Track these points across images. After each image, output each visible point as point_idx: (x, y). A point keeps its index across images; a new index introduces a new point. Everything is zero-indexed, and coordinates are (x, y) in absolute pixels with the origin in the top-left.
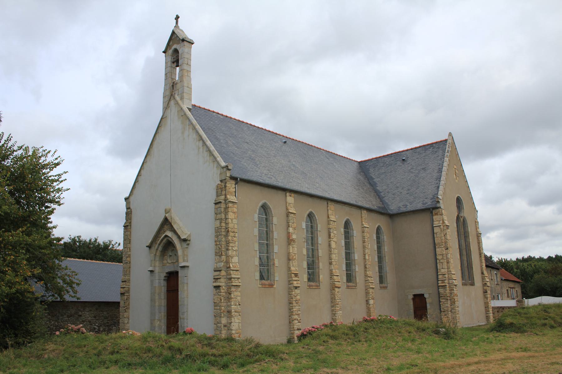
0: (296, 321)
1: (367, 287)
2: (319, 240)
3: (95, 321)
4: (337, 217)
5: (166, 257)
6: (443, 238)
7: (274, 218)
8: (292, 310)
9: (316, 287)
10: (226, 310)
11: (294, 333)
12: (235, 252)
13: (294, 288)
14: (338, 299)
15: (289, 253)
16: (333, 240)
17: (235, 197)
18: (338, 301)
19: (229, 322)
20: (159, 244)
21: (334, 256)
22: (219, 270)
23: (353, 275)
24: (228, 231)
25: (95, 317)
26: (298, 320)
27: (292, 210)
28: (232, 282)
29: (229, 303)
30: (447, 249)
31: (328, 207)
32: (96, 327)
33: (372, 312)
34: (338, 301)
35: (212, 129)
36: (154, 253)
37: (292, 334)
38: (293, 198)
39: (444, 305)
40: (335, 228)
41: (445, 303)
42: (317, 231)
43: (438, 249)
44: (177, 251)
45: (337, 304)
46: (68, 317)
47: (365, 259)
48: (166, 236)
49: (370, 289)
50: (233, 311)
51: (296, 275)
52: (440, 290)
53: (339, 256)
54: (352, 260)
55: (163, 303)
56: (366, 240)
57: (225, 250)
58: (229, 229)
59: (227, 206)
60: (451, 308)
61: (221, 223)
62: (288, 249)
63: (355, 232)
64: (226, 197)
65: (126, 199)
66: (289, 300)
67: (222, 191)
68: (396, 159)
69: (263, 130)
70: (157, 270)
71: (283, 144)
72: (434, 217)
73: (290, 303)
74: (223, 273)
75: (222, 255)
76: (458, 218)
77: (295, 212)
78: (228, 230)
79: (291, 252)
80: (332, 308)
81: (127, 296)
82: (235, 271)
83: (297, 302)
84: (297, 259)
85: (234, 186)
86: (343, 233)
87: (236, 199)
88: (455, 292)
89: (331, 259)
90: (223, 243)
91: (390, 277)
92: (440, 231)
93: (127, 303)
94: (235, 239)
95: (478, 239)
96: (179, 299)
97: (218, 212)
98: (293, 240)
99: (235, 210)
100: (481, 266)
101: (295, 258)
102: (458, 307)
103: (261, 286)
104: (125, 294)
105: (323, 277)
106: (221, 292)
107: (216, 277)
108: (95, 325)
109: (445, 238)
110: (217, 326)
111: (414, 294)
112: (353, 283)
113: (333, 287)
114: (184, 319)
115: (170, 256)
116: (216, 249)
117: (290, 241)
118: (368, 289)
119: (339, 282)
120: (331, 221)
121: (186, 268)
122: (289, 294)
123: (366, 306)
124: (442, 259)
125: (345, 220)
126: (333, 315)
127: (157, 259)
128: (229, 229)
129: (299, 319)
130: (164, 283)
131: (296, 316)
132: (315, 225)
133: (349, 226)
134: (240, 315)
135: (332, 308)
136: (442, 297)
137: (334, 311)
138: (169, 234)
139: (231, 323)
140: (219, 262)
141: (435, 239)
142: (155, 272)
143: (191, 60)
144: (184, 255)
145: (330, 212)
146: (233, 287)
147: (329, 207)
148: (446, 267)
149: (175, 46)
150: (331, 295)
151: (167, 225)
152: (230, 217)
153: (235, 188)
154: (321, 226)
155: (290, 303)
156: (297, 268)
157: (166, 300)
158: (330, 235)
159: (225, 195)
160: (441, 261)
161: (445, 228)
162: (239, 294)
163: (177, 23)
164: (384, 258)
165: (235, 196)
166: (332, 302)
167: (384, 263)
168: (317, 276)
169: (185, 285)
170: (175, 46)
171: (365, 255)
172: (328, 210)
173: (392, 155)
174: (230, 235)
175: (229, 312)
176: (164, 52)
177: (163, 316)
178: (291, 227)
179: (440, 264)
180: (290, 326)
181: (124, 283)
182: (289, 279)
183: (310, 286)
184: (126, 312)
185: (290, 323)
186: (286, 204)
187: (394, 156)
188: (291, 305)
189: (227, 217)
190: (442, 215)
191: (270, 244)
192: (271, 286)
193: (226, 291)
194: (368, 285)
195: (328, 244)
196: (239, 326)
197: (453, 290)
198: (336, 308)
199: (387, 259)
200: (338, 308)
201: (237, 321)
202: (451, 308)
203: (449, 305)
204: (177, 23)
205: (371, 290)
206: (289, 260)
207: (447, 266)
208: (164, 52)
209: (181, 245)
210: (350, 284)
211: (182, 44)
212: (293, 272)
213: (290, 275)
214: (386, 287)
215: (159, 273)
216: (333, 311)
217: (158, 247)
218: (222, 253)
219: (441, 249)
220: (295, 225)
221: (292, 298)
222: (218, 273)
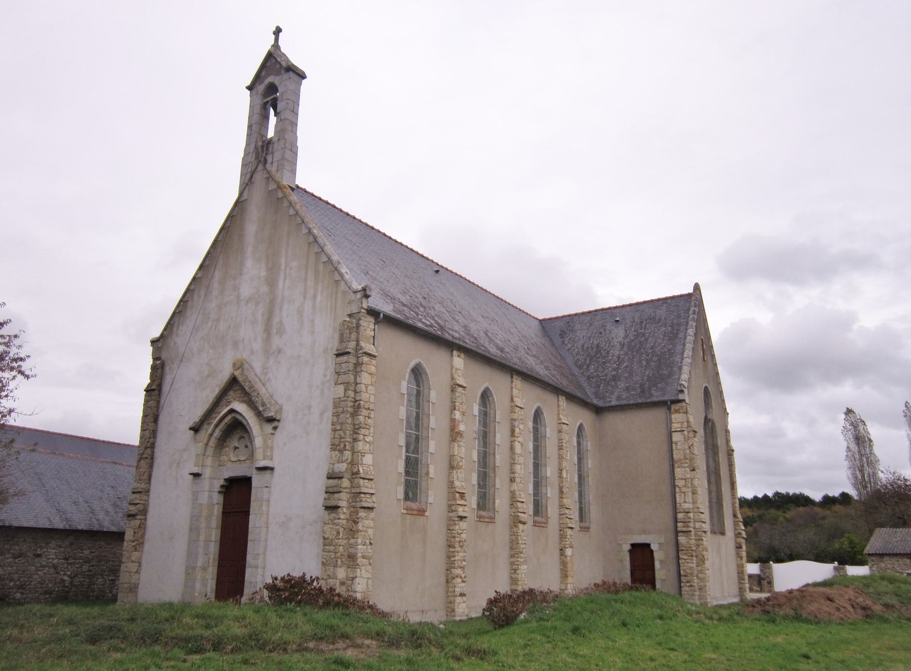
0: (459, 580)
1: (562, 526)
2: (497, 437)
3: (65, 566)
4: (524, 401)
5: (227, 449)
6: (688, 451)
7: (431, 391)
8: (452, 559)
9: (489, 520)
10: (346, 553)
11: (455, 601)
12: (368, 445)
13: (459, 519)
14: (522, 544)
15: (451, 457)
16: (519, 439)
17: (372, 346)
18: (522, 546)
19: (351, 576)
20: (217, 426)
21: (518, 468)
22: (338, 476)
23: (542, 503)
24: (359, 407)
25: (66, 559)
26: (461, 577)
27: (461, 381)
28: (361, 501)
29: (352, 541)
30: (694, 470)
31: (512, 382)
32: (66, 578)
33: (569, 569)
34: (522, 546)
35: (328, 228)
36: (205, 441)
37: (450, 603)
38: (463, 361)
39: (686, 564)
40: (522, 419)
41: (687, 561)
42: (495, 421)
43: (679, 469)
44: (251, 440)
45: (521, 553)
46: (15, 557)
47: (560, 477)
48: (232, 411)
49: (567, 529)
50: (359, 555)
51: (462, 495)
52: (679, 538)
53: (524, 469)
54: (541, 478)
55: (214, 535)
56: (564, 444)
57: (351, 441)
58: (361, 402)
59: (360, 360)
60: (698, 570)
61: (346, 390)
62: (450, 448)
63: (548, 429)
64: (358, 345)
65: (153, 342)
66: (447, 540)
67: (350, 333)
68: (603, 319)
69: (403, 247)
70: (207, 473)
71: (434, 273)
72: (674, 416)
73: (450, 546)
74: (345, 483)
75: (345, 448)
76: (706, 418)
77: (465, 385)
78: (359, 404)
79: (456, 454)
80: (512, 560)
81: (140, 519)
82: (367, 481)
83: (461, 544)
84: (464, 467)
85: (372, 326)
86: (531, 430)
87: (375, 350)
88: (705, 543)
89: (514, 473)
90: (349, 427)
91: (594, 513)
92: (683, 440)
93: (139, 535)
94: (370, 421)
95: (729, 459)
96: (250, 530)
97: (342, 371)
98: (460, 434)
99: (373, 369)
100: (733, 504)
101: (462, 466)
102: (708, 570)
103: (405, 512)
104: (137, 517)
105: (501, 502)
106: (339, 519)
107: (331, 490)
108: (65, 574)
109: (690, 451)
110: (327, 583)
111: (632, 542)
112: (542, 517)
113: (516, 521)
114: (257, 567)
115: (236, 448)
116: (334, 438)
117: (455, 434)
118: (565, 530)
119: (525, 513)
120: (517, 406)
121: (268, 472)
122: (449, 530)
123: (560, 559)
124: (684, 487)
125: (535, 407)
126: (513, 571)
127: (210, 451)
128: (361, 402)
129: (463, 576)
130: (218, 499)
131: (459, 570)
132: (492, 412)
133: (540, 418)
134: (370, 564)
135: (512, 560)
136: (682, 550)
137: (515, 564)
138: (241, 407)
139: (353, 579)
140: (338, 462)
141: (674, 452)
142: (203, 477)
143: (299, 105)
144: (266, 447)
145: (515, 392)
146: (362, 510)
147: (514, 384)
148: (690, 500)
149: (270, 79)
150: (511, 535)
151: (235, 391)
152: (364, 381)
153: (374, 330)
154: (500, 413)
155: (450, 546)
156: (463, 484)
157: (220, 531)
158: (513, 431)
159: (358, 341)
160: (684, 489)
161: (691, 435)
162: (372, 524)
163: (277, 40)
164: (586, 479)
165: (374, 345)
166: (511, 548)
167: (587, 486)
168: (491, 501)
169: (264, 502)
170: (270, 79)
171: (561, 470)
172: (512, 388)
173: (597, 313)
174: (363, 414)
175: (352, 557)
176: (250, 88)
177: (211, 561)
178: (459, 410)
179: (680, 495)
180: (448, 587)
181: (138, 496)
182: (450, 502)
183: (479, 517)
184: (136, 550)
185: (447, 582)
186: (452, 369)
187: (601, 314)
188: (451, 550)
189: (358, 381)
190: (686, 413)
191: (422, 436)
192: (421, 512)
193: (348, 516)
194: (565, 522)
195: (509, 447)
196: (367, 585)
197: (702, 540)
198: (519, 559)
199: (591, 481)
200: (522, 560)
201: (365, 574)
202: (698, 570)
203: (694, 565)
204: (277, 40)
205: (569, 532)
206: (452, 468)
207: (693, 499)
208: (250, 88)
209: (261, 428)
210: (538, 519)
211: (286, 76)
212: (458, 490)
213: (454, 495)
214: (589, 528)
215: (210, 478)
216: (512, 564)
217: (213, 431)
218: (345, 446)
219: (683, 469)
220: (464, 407)
221: (454, 537)
222: (336, 481)
